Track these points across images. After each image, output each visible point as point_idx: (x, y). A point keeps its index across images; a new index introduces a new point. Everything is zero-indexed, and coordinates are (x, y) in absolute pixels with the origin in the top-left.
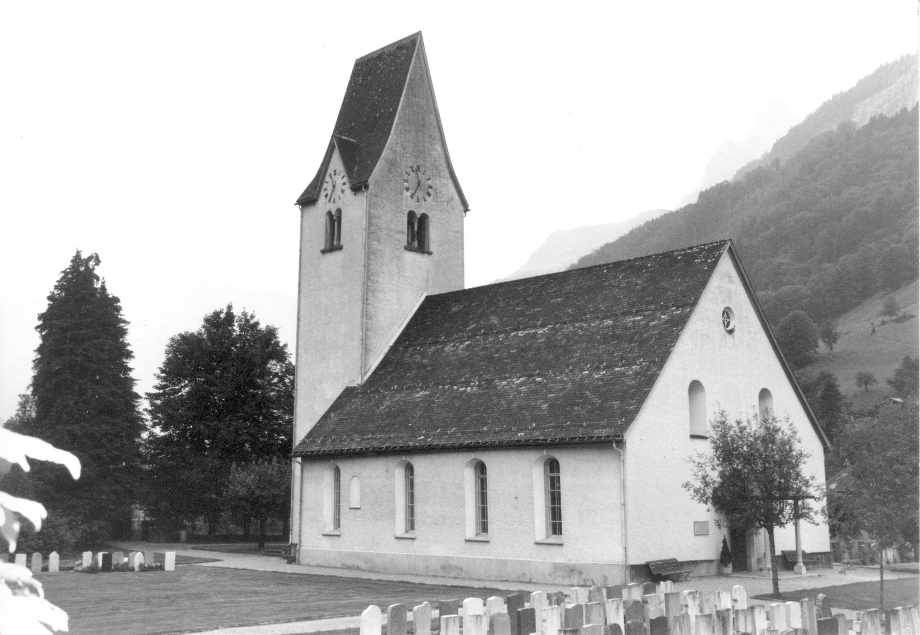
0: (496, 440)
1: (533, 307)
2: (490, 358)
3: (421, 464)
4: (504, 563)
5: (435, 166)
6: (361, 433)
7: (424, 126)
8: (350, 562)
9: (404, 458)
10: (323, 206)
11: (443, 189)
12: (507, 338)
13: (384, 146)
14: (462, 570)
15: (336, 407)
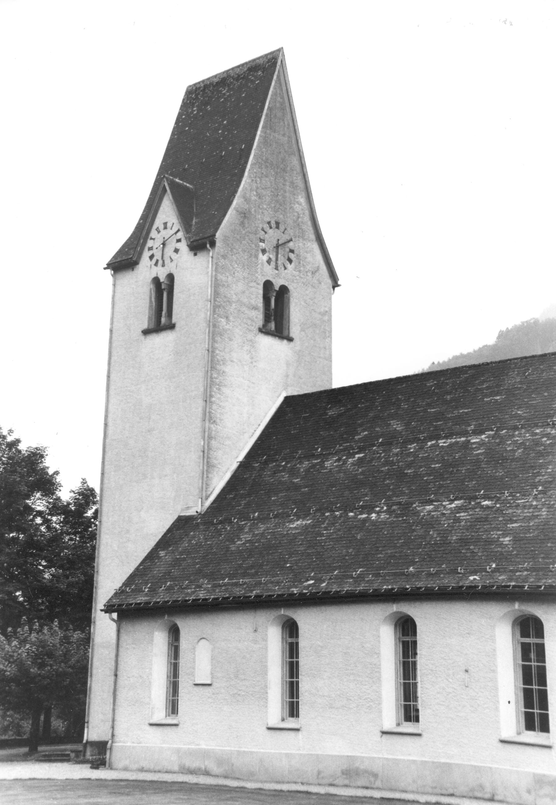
0: (434, 584)
1: (457, 408)
2: (400, 476)
3: (309, 621)
4: (447, 767)
5: (298, 225)
6: (212, 577)
7: (284, 170)
8: (195, 764)
9: (282, 612)
10: (146, 271)
11: (308, 255)
12: (421, 448)
13: (236, 192)
14: (376, 776)
15: (166, 541)
